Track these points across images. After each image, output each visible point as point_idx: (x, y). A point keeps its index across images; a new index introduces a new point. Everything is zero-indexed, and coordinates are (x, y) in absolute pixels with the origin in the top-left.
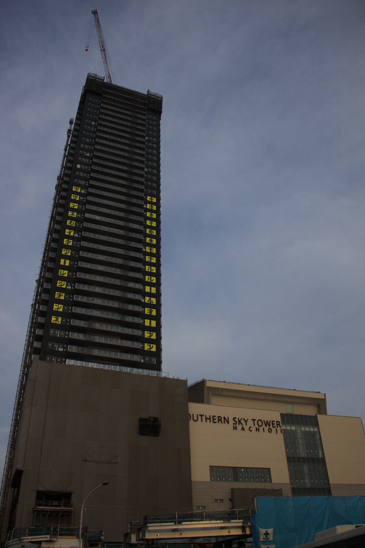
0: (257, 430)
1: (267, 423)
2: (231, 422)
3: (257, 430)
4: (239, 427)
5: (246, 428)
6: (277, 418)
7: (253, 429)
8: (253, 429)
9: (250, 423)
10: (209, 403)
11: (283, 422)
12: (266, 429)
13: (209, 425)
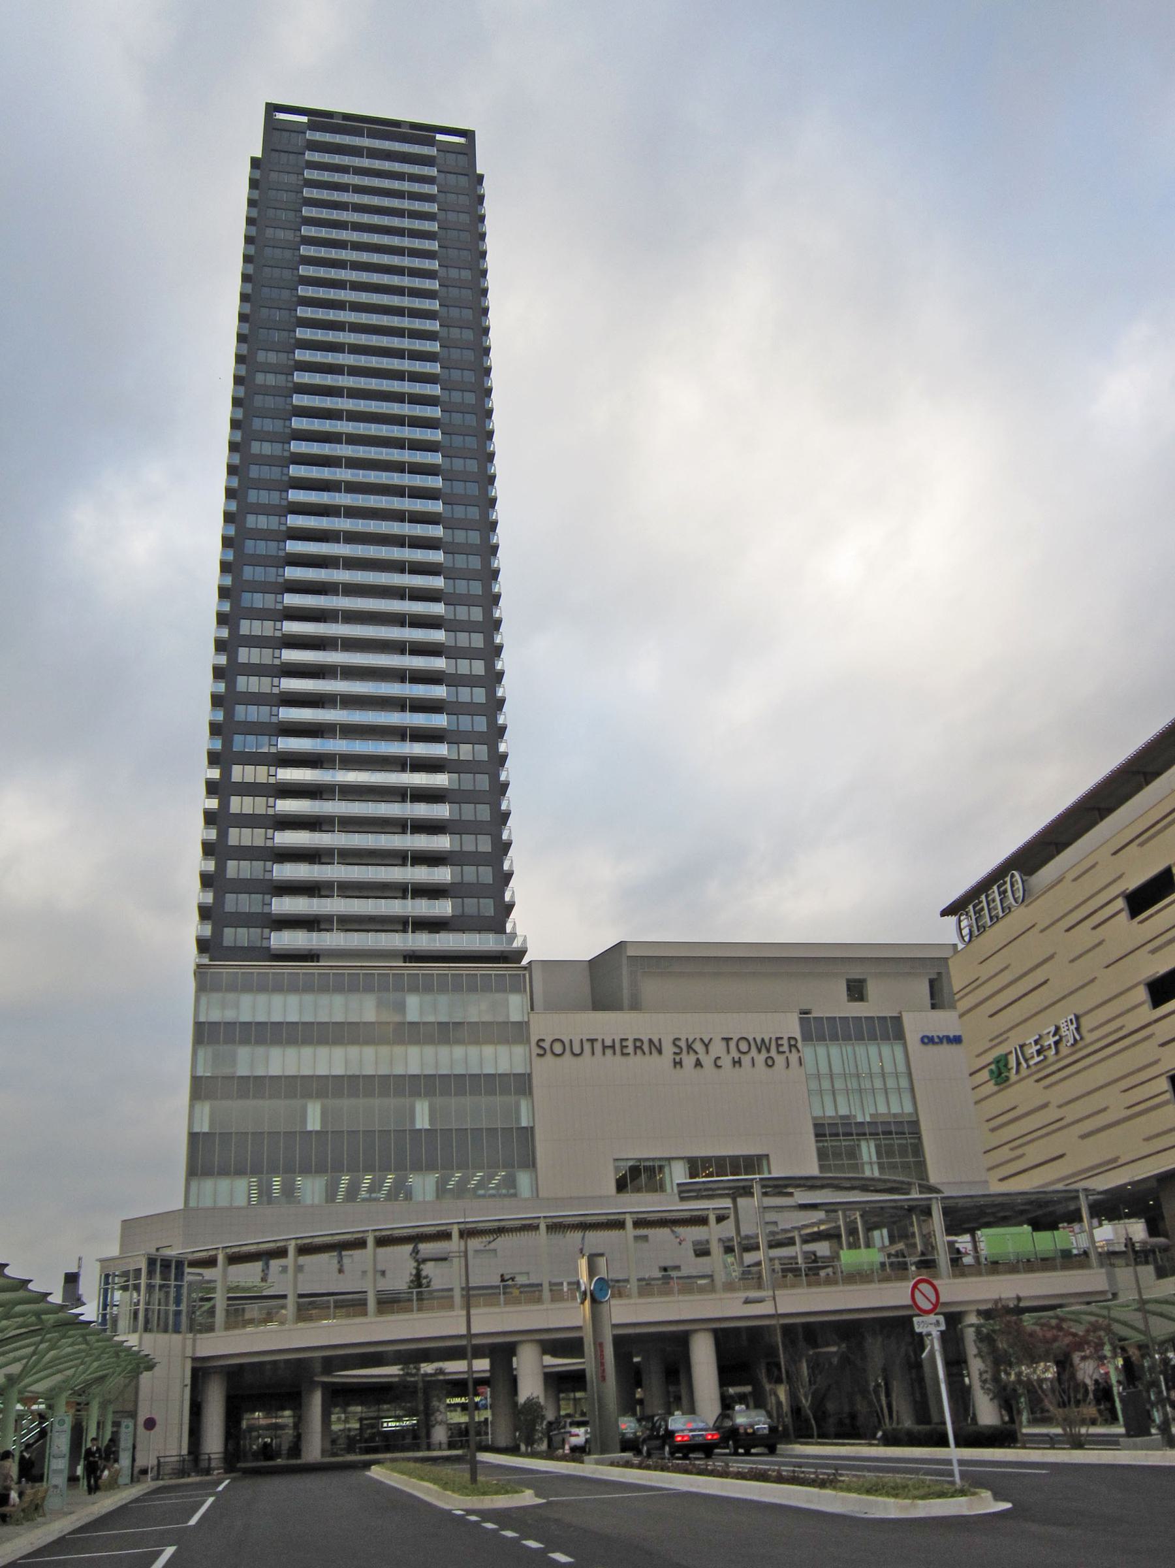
0: (737, 1063)
1: (763, 1046)
2: (668, 1049)
3: (737, 1063)
4: (689, 1060)
5: (707, 1061)
6: (791, 1026)
7: (726, 1061)
8: (726, 1061)
9: (718, 1048)
10: (635, 1006)
11: (807, 1037)
12: (760, 1058)
13: (613, 1061)
